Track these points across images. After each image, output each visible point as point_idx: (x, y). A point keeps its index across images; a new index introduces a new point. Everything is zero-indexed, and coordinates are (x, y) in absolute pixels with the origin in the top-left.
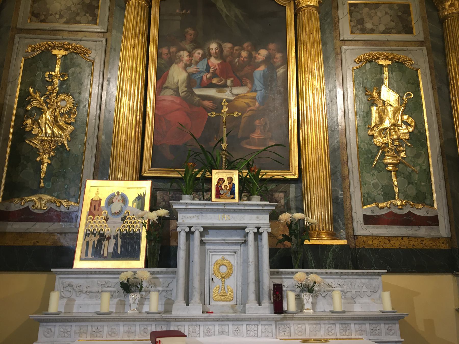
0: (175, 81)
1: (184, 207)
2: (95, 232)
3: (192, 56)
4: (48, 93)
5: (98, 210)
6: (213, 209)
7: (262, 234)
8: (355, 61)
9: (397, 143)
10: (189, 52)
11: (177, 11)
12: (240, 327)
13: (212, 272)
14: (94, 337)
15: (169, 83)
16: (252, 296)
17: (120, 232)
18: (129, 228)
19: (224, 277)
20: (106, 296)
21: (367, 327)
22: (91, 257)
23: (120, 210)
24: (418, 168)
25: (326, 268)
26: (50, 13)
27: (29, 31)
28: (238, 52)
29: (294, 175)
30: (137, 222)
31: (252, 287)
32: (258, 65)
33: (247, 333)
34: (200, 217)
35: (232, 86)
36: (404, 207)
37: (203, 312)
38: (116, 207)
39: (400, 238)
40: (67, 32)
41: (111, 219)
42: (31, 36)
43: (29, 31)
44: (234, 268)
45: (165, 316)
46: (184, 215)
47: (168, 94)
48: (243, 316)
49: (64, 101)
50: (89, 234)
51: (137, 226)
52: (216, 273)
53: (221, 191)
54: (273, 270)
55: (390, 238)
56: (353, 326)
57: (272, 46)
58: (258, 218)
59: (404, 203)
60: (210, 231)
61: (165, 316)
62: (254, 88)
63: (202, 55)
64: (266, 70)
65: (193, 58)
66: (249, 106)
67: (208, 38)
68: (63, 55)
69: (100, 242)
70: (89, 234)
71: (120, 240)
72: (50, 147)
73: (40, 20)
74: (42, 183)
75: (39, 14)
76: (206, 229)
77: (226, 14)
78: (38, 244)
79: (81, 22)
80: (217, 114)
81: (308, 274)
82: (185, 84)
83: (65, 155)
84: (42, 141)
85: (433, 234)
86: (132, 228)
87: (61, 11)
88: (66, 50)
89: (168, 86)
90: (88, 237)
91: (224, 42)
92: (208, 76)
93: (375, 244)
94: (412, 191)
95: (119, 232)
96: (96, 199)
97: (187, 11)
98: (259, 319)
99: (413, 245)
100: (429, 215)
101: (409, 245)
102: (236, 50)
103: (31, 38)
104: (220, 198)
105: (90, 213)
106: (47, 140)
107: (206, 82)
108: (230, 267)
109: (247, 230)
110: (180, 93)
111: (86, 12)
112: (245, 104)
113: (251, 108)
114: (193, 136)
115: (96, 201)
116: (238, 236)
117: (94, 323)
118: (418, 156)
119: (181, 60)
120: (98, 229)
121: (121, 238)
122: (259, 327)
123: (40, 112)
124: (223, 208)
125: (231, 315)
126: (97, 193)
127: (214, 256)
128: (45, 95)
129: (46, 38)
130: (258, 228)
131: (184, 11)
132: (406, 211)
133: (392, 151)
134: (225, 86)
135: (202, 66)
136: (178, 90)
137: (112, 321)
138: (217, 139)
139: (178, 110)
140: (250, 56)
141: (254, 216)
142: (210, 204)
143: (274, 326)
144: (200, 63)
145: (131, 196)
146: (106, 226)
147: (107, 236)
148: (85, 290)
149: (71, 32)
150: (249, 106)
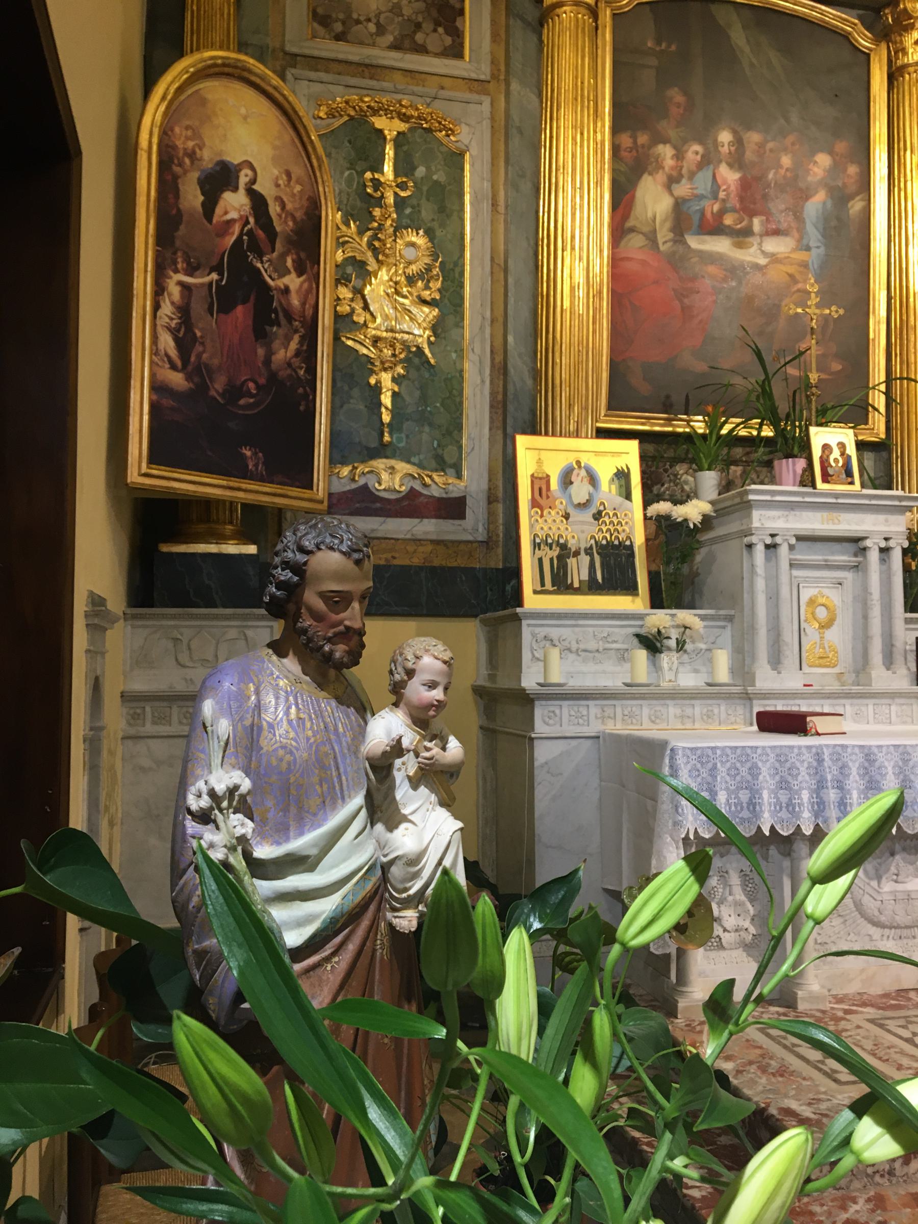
0: (650, 215)
1: (768, 498)
2: (550, 541)
3: (683, 158)
5: (548, 497)
7: (754, 549)
10: (675, 147)
11: (649, 44)
12: (863, 709)
14: (628, 724)
16: (876, 656)
17: (596, 542)
18: (611, 535)
22: (551, 589)
23: (587, 497)
26: (355, 16)
27: (315, 62)
30: (623, 523)
33: (874, 718)
38: (580, 490)
40: (400, 72)
42: (322, 75)
43: (315, 62)
46: (763, 512)
49: (412, 248)
50: (539, 544)
51: (624, 531)
53: (829, 469)
58: (886, 521)
62: (805, 242)
63: (703, 156)
65: (685, 164)
68: (399, 133)
70: (539, 544)
71: (597, 559)
72: (394, 355)
73: (333, 34)
74: (386, 434)
75: (329, 17)
78: (396, 562)
79: (430, 48)
82: (668, 225)
83: (427, 375)
84: (376, 340)
86: (616, 534)
87: (380, 13)
88: (404, 118)
89: (635, 227)
90: (539, 549)
91: (749, 128)
92: (716, 208)
95: (593, 542)
96: (540, 475)
97: (669, 46)
98: (893, 695)
102: (771, 150)
103: (322, 82)
104: (828, 482)
105: (534, 504)
106: (386, 338)
107: (711, 220)
109: (868, 543)
111: (437, 24)
114: (758, 354)
115: (541, 479)
116: (843, 554)
117: (624, 702)
120: (554, 534)
121: (598, 553)
122: (893, 708)
124: (834, 501)
126: (539, 462)
127: (805, 589)
128: (369, 229)
129: (357, 85)
131: (664, 46)
136: (656, 237)
137: (656, 699)
141: (881, 517)
142: (815, 495)
144: (700, 175)
145: (605, 472)
147: (573, 549)
148: (574, 646)
149: (409, 74)
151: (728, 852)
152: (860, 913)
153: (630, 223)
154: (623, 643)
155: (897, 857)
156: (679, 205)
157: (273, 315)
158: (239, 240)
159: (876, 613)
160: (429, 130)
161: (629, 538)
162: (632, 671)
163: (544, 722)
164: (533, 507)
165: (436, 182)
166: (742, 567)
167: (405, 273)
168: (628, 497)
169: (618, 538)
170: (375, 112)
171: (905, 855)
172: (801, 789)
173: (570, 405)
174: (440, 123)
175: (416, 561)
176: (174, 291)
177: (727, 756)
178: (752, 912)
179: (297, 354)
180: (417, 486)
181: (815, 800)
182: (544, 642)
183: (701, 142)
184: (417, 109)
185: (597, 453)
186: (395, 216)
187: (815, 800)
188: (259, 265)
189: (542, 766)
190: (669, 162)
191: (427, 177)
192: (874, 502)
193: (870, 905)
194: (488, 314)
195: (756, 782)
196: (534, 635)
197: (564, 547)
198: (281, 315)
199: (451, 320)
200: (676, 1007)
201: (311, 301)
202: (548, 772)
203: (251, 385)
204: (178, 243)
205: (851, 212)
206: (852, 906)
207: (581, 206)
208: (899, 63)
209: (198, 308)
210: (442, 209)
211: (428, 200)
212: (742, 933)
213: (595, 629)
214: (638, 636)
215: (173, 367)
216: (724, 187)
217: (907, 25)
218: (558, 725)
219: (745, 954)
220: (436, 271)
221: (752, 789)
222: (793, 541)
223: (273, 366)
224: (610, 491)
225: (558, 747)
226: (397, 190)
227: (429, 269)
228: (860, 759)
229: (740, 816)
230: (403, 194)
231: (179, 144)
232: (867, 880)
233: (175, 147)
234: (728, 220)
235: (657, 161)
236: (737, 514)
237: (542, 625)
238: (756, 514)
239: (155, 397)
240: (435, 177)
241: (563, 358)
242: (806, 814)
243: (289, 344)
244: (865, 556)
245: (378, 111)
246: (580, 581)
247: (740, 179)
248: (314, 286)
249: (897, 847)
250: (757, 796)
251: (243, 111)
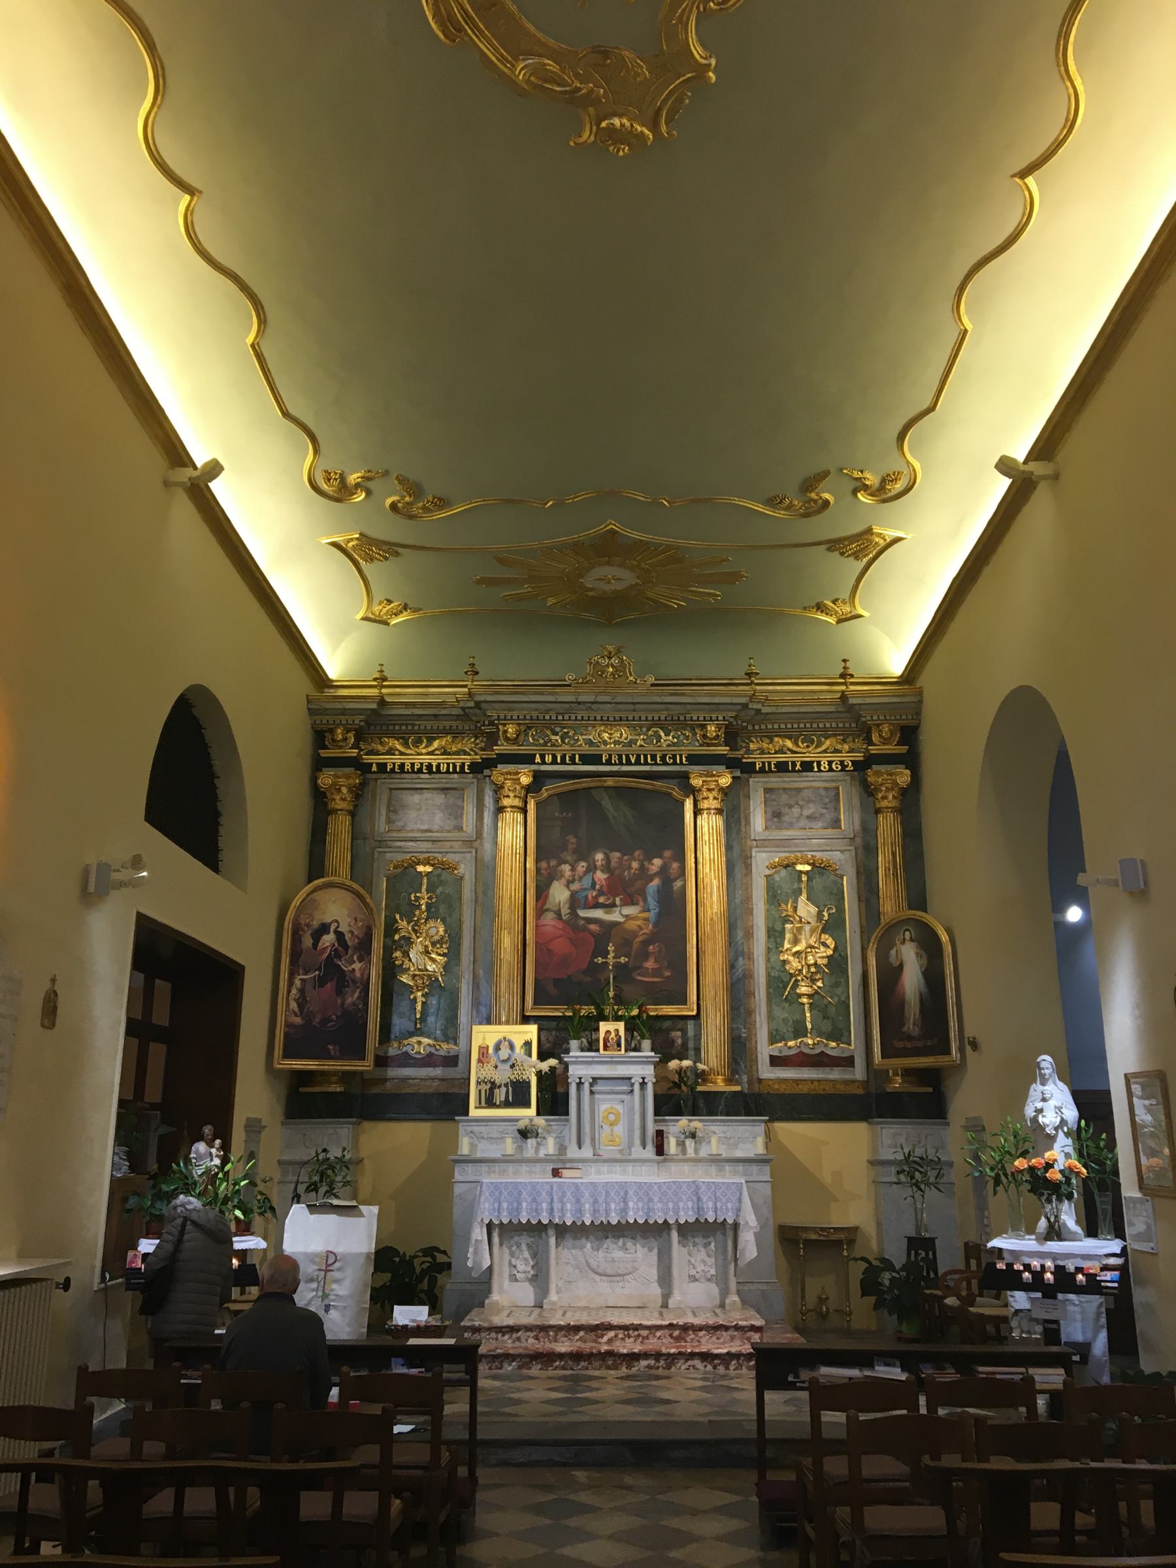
0: (557, 901)
1: (574, 1059)
4: (416, 919)
8: (767, 867)
9: (813, 970)
10: (571, 865)
11: (557, 814)
13: (601, 1119)
16: (637, 1141)
19: (612, 1124)
20: (509, 1141)
21: (740, 1168)
24: (836, 999)
25: (717, 1116)
28: (627, 863)
29: (692, 1011)
31: (637, 1133)
32: (651, 879)
35: (622, 906)
36: (816, 1046)
37: (594, 1155)
38: (504, 1053)
41: (501, 1066)
44: (622, 1116)
45: (561, 1157)
47: (549, 918)
48: (630, 1158)
52: (605, 1121)
54: (657, 1118)
55: (799, 1082)
56: (727, 1167)
57: (667, 854)
59: (816, 1042)
60: (599, 1082)
61: (561, 1157)
63: (587, 868)
64: (660, 885)
66: (641, 929)
67: (593, 848)
69: (492, 1090)
71: (510, 1089)
72: (423, 983)
76: (595, 1080)
77: (614, 816)
78: (421, 1091)
80: (604, 960)
81: (690, 1121)
82: (567, 906)
84: (414, 976)
85: (847, 1077)
91: (611, 851)
92: (594, 894)
93: (783, 1089)
94: (827, 1026)
99: (824, 1090)
100: (844, 1056)
101: (819, 1089)
102: (626, 861)
105: (479, 1061)
108: (618, 1115)
109: (633, 1081)
110: (563, 915)
113: (645, 931)
115: (484, 1048)
116: (623, 1086)
118: (836, 985)
119: (562, 876)
123: (408, 941)
125: (619, 1156)
126: (484, 1039)
130: (643, 1078)
131: (564, 814)
132: (817, 1051)
133: (807, 978)
134: (613, 905)
135: (587, 882)
138: (569, 1259)
139: (560, 937)
140: (642, 868)
143: (656, 1167)
144: (585, 879)
150: (641, 929)
151: (522, 1235)
155: (608, 1240)
158: (330, 954)
162: (711, 1149)
171: (613, 1240)
172: (542, 1202)
175: (431, 1090)
176: (298, 983)
178: (532, 1263)
180: (433, 1050)
185: (515, 1033)
188: (340, 963)
189: (457, 1196)
193: (593, 1264)
194: (472, 959)
201: (367, 972)
203: (333, 1017)
204: (300, 963)
209: (308, 987)
215: (296, 1015)
223: (345, 1006)
228: (573, 1189)
231: (303, 922)
233: (300, 924)
239: (287, 1030)
242: (545, 1214)
246: (500, 1102)
249: (610, 1235)
251: (333, 899)
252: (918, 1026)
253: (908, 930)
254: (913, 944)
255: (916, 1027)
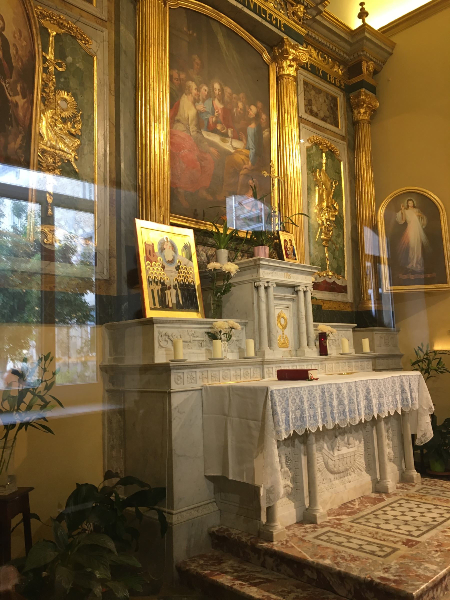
0: (186, 116)
5: (154, 256)
6: (275, 266)
15: (181, 116)
18: (185, 279)
22: (159, 307)
30: (190, 272)
34: (274, 274)
38: (169, 254)
39: (329, 302)
46: (264, 270)
49: (64, 102)
51: (190, 277)
56: (353, 364)
63: (208, 92)
66: (245, 164)
70: (151, 282)
72: (54, 163)
85: (345, 300)
90: (152, 285)
91: (226, 85)
95: (176, 282)
96: (149, 244)
100: (343, 285)
105: (147, 259)
106: (49, 151)
109: (300, 288)
112: (241, 161)
115: (149, 245)
121: (180, 289)
131: (191, 32)
132: (332, 281)
144: (207, 102)
146: (164, 274)
147: (168, 286)
152: (327, 469)
153: (177, 118)
154: (201, 337)
155: (338, 438)
156: (199, 114)
157: (10, 119)
159: (303, 321)
160: (75, 38)
161: (193, 281)
163: (176, 383)
164: (147, 261)
165: (78, 68)
166: (253, 298)
167: (60, 115)
168: (191, 259)
169: (187, 281)
170: (44, 17)
173: (160, 206)
174: (81, 36)
177: (284, 393)
179: (20, 148)
181: (322, 413)
182: (165, 337)
183: (207, 86)
184: (68, 23)
186: (54, 80)
187: (322, 413)
188: (4, 84)
189: (175, 409)
190: (194, 91)
191: (72, 64)
192: (303, 269)
195: (303, 406)
196: (159, 333)
197: (163, 284)
198: (13, 119)
199: (86, 149)
200: (272, 535)
201: (28, 116)
202: (178, 412)
205: (264, 136)
206: (324, 465)
207: (163, 102)
208: (280, 73)
210: (82, 84)
211: (74, 77)
212: (287, 488)
213: (188, 329)
214: (208, 333)
216: (217, 111)
217: (285, 57)
218: (182, 384)
219: (288, 499)
220: (78, 118)
221: (301, 409)
222: (275, 285)
224: (182, 256)
225: (184, 396)
226: (57, 67)
227: (74, 116)
229: (297, 424)
230: (60, 69)
232: (329, 451)
234: (219, 127)
235: (189, 89)
236: (248, 271)
237: (164, 327)
238: (261, 271)
240: (78, 65)
241: (156, 180)
242: (320, 420)
243: (16, 140)
244: (297, 294)
245: (46, 17)
246: (172, 304)
247: (223, 108)
248: (30, 107)
250: (304, 413)
252: (420, 265)
253: (410, 200)
254: (415, 210)
255: (418, 265)
